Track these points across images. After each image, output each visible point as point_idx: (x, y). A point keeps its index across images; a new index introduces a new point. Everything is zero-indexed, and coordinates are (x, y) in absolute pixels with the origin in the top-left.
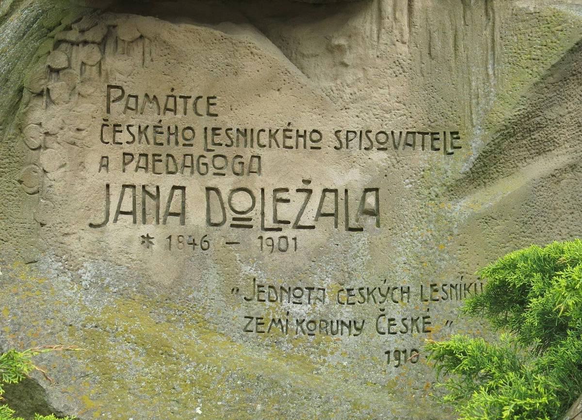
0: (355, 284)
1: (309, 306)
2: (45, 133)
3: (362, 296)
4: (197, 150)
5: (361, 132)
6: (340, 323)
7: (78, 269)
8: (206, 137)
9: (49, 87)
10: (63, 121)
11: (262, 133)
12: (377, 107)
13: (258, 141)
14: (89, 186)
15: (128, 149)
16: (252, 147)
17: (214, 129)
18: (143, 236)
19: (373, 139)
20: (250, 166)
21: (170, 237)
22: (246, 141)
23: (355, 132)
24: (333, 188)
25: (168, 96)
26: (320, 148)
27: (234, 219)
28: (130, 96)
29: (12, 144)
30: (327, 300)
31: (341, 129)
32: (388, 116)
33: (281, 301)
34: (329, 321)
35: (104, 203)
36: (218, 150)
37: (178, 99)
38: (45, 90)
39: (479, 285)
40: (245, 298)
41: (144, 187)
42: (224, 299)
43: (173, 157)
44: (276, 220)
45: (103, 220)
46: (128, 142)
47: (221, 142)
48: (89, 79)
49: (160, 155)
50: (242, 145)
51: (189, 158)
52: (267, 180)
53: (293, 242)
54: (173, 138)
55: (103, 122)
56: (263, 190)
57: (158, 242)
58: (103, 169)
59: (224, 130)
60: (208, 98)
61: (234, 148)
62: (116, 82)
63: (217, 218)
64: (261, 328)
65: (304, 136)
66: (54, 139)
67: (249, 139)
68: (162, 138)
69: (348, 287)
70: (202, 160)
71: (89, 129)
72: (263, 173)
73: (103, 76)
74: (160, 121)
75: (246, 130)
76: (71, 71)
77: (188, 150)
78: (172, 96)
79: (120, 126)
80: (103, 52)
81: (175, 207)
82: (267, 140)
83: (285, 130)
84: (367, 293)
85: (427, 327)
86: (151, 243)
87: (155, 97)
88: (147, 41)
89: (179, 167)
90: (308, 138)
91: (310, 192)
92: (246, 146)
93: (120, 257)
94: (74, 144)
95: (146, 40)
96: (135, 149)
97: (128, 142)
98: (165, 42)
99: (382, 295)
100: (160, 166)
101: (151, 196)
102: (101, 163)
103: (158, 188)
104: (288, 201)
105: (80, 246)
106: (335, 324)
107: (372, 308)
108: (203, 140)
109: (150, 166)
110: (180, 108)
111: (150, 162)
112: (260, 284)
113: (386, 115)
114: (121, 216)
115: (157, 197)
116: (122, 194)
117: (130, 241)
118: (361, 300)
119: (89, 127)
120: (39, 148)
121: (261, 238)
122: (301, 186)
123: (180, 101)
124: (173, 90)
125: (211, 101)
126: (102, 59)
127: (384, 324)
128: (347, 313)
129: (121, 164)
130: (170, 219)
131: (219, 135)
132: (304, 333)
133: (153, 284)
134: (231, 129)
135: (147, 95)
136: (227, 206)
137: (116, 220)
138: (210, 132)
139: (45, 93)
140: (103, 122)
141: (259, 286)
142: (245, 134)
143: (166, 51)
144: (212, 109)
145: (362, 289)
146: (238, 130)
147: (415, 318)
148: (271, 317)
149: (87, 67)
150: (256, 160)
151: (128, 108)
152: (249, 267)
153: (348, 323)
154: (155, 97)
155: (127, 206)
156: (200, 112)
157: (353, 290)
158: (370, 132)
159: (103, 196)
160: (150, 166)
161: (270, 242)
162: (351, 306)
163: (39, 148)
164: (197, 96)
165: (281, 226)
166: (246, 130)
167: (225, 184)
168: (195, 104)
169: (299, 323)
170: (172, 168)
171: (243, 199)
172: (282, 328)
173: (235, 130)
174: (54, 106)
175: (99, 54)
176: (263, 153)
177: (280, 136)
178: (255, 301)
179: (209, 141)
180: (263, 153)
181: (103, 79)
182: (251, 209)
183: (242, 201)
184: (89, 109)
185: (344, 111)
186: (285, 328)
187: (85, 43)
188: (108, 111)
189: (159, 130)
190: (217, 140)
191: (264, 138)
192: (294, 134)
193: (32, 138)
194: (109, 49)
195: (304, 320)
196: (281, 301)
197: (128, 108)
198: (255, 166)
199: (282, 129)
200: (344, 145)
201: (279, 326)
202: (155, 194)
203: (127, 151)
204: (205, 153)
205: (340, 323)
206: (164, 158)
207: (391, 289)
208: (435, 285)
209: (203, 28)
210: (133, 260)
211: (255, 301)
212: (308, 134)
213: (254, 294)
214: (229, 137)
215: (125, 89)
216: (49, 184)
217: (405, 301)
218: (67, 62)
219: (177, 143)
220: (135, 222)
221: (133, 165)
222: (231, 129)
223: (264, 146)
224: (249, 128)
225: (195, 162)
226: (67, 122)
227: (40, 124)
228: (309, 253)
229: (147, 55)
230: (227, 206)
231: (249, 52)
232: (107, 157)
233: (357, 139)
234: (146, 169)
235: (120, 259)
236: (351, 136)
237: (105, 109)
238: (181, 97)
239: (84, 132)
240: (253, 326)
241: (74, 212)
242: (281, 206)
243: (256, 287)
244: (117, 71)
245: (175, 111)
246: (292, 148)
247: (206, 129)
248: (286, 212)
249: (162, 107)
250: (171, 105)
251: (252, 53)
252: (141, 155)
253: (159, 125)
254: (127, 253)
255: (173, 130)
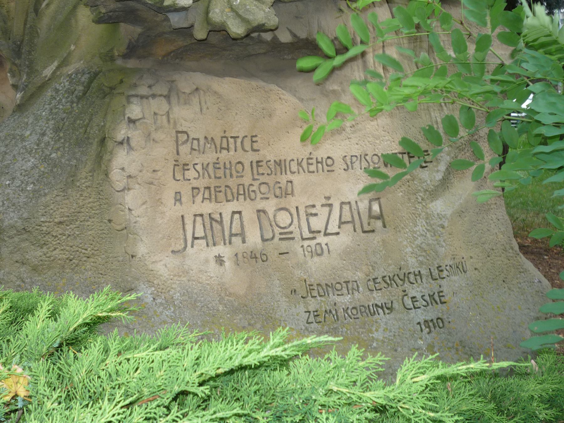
0: (379, 273)
1: (349, 296)
2: (127, 177)
3: (385, 282)
4: (247, 180)
5: (361, 156)
6: (374, 306)
7: (169, 291)
8: (252, 168)
9: (129, 136)
10: (142, 164)
11: (292, 162)
12: (370, 136)
13: (290, 169)
14: (168, 219)
15: (195, 184)
16: (286, 174)
17: (258, 162)
18: (216, 256)
19: (370, 161)
20: (286, 189)
21: (236, 255)
22: (281, 169)
23: (356, 156)
24: (347, 201)
25: (222, 137)
26: (333, 171)
27: (281, 234)
28: (194, 139)
29: (101, 188)
30: (361, 289)
31: (346, 154)
32: (378, 142)
33: (328, 295)
34: (367, 305)
35: (182, 231)
36: (262, 179)
37: (230, 139)
38: (126, 139)
39: (464, 263)
40: (302, 297)
41: (210, 214)
42: (287, 300)
43: (230, 189)
44: (311, 232)
45: (183, 246)
46: (195, 178)
47: (264, 172)
48: (161, 127)
49: (220, 187)
50: (279, 173)
51: (241, 187)
52: (299, 200)
53: (326, 247)
54: (228, 171)
55: (175, 163)
56: (297, 208)
57: (229, 259)
58: (178, 204)
59: (265, 162)
60: (252, 137)
61: (273, 176)
62: (183, 128)
63: (268, 235)
64: (319, 319)
65: (321, 163)
66: (134, 180)
67: (283, 168)
68: (220, 173)
69: (374, 277)
70: (252, 188)
71: (163, 170)
72: (296, 194)
73: (172, 124)
74: (218, 158)
75: (280, 161)
76: (145, 121)
77: (240, 181)
78: (225, 137)
79: (188, 165)
80: (169, 103)
81: (236, 229)
82: (297, 167)
83: (308, 159)
84: (389, 281)
85: (443, 299)
86: (223, 261)
87: (212, 138)
88: (202, 92)
89: (235, 195)
90: (324, 164)
91: (330, 205)
92: (281, 174)
93: (201, 276)
94: (152, 183)
95: (201, 91)
96: (201, 183)
97: (195, 178)
98: (215, 92)
99: (401, 280)
100: (221, 196)
101: (216, 221)
102: (175, 198)
103: (221, 214)
104: (316, 215)
105: (167, 270)
106: (371, 308)
107: (397, 291)
108: (250, 172)
109: (213, 197)
110: (232, 146)
111: (213, 193)
112: (310, 284)
113: (376, 141)
114: (196, 241)
115: (221, 223)
116: (194, 221)
117: (207, 261)
118: (386, 286)
119: (163, 168)
120: (123, 190)
121: (302, 246)
122: (324, 201)
123: (231, 141)
124: (225, 132)
125: (254, 139)
126: (170, 109)
127: (408, 302)
128: (378, 298)
129: (192, 197)
130: (234, 239)
131: (262, 166)
132: (351, 318)
133: (230, 295)
134: (270, 161)
135: (206, 138)
136: (273, 223)
137: (192, 246)
138: (254, 165)
139: (125, 141)
140: (175, 163)
141: (309, 285)
142: (280, 165)
143: (218, 100)
144: (255, 146)
145: (385, 277)
146: (275, 161)
147: (432, 294)
148: (324, 309)
149: (159, 117)
150: (289, 184)
151: (192, 149)
152: (300, 272)
153: (380, 305)
154: (212, 138)
155: (200, 232)
156: (247, 149)
157: (377, 278)
158: (367, 155)
159: (179, 226)
160: (213, 197)
161: (309, 249)
162: (379, 291)
163: (123, 190)
164: (244, 135)
165: (315, 235)
166: (280, 161)
167: (270, 206)
168: (242, 142)
169: (346, 310)
170: (230, 197)
171: (284, 217)
172: (333, 316)
173: (272, 161)
174: (133, 152)
175: (167, 105)
176: (296, 179)
177: (304, 164)
178: (310, 298)
179: (255, 172)
180: (296, 179)
181: (171, 127)
182: (290, 225)
183: (283, 219)
184: (162, 151)
185: (347, 140)
186: (336, 317)
187: (154, 96)
188: (178, 153)
189: (218, 166)
190: (261, 170)
191: (294, 167)
192: (314, 161)
193: (117, 181)
194: (174, 100)
195: (348, 308)
196: (328, 295)
197: (192, 149)
198: (290, 190)
199: (306, 158)
200: (350, 167)
201: (331, 315)
202: (219, 220)
203: (195, 185)
204: (253, 183)
205: (374, 306)
206: (223, 189)
207: (407, 274)
208: (440, 267)
209: (242, 80)
210: (211, 278)
211: (310, 298)
212: (324, 160)
213: (307, 292)
214: (269, 167)
215: (189, 133)
216: (135, 221)
217: (419, 281)
218: (142, 113)
219: (231, 176)
220: (208, 245)
221: (199, 198)
222: (270, 161)
223: (294, 173)
224: (283, 158)
225: (246, 190)
226: (145, 164)
227: (123, 169)
228: (340, 254)
229: (203, 104)
230: (273, 223)
231: (278, 97)
232: (179, 193)
233: (358, 162)
234: (210, 199)
235: (201, 278)
236: (354, 159)
237: (175, 152)
238: (232, 137)
239: (159, 172)
240: (312, 319)
241: (159, 242)
242: (312, 220)
243: (308, 286)
244: (182, 118)
245: (228, 149)
246: (313, 172)
247: (252, 162)
248: (317, 223)
249: (218, 147)
250: (225, 145)
251: (280, 98)
252: (205, 188)
253: (217, 162)
254: (206, 272)
255: (228, 166)
